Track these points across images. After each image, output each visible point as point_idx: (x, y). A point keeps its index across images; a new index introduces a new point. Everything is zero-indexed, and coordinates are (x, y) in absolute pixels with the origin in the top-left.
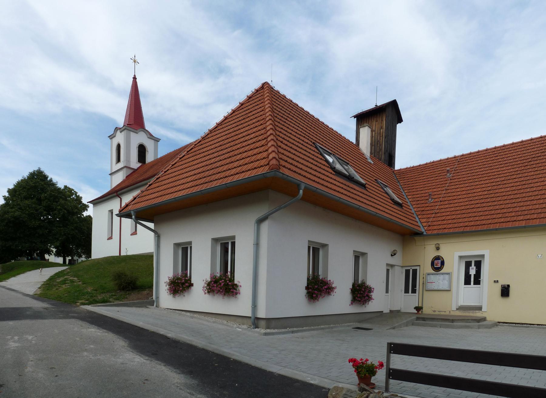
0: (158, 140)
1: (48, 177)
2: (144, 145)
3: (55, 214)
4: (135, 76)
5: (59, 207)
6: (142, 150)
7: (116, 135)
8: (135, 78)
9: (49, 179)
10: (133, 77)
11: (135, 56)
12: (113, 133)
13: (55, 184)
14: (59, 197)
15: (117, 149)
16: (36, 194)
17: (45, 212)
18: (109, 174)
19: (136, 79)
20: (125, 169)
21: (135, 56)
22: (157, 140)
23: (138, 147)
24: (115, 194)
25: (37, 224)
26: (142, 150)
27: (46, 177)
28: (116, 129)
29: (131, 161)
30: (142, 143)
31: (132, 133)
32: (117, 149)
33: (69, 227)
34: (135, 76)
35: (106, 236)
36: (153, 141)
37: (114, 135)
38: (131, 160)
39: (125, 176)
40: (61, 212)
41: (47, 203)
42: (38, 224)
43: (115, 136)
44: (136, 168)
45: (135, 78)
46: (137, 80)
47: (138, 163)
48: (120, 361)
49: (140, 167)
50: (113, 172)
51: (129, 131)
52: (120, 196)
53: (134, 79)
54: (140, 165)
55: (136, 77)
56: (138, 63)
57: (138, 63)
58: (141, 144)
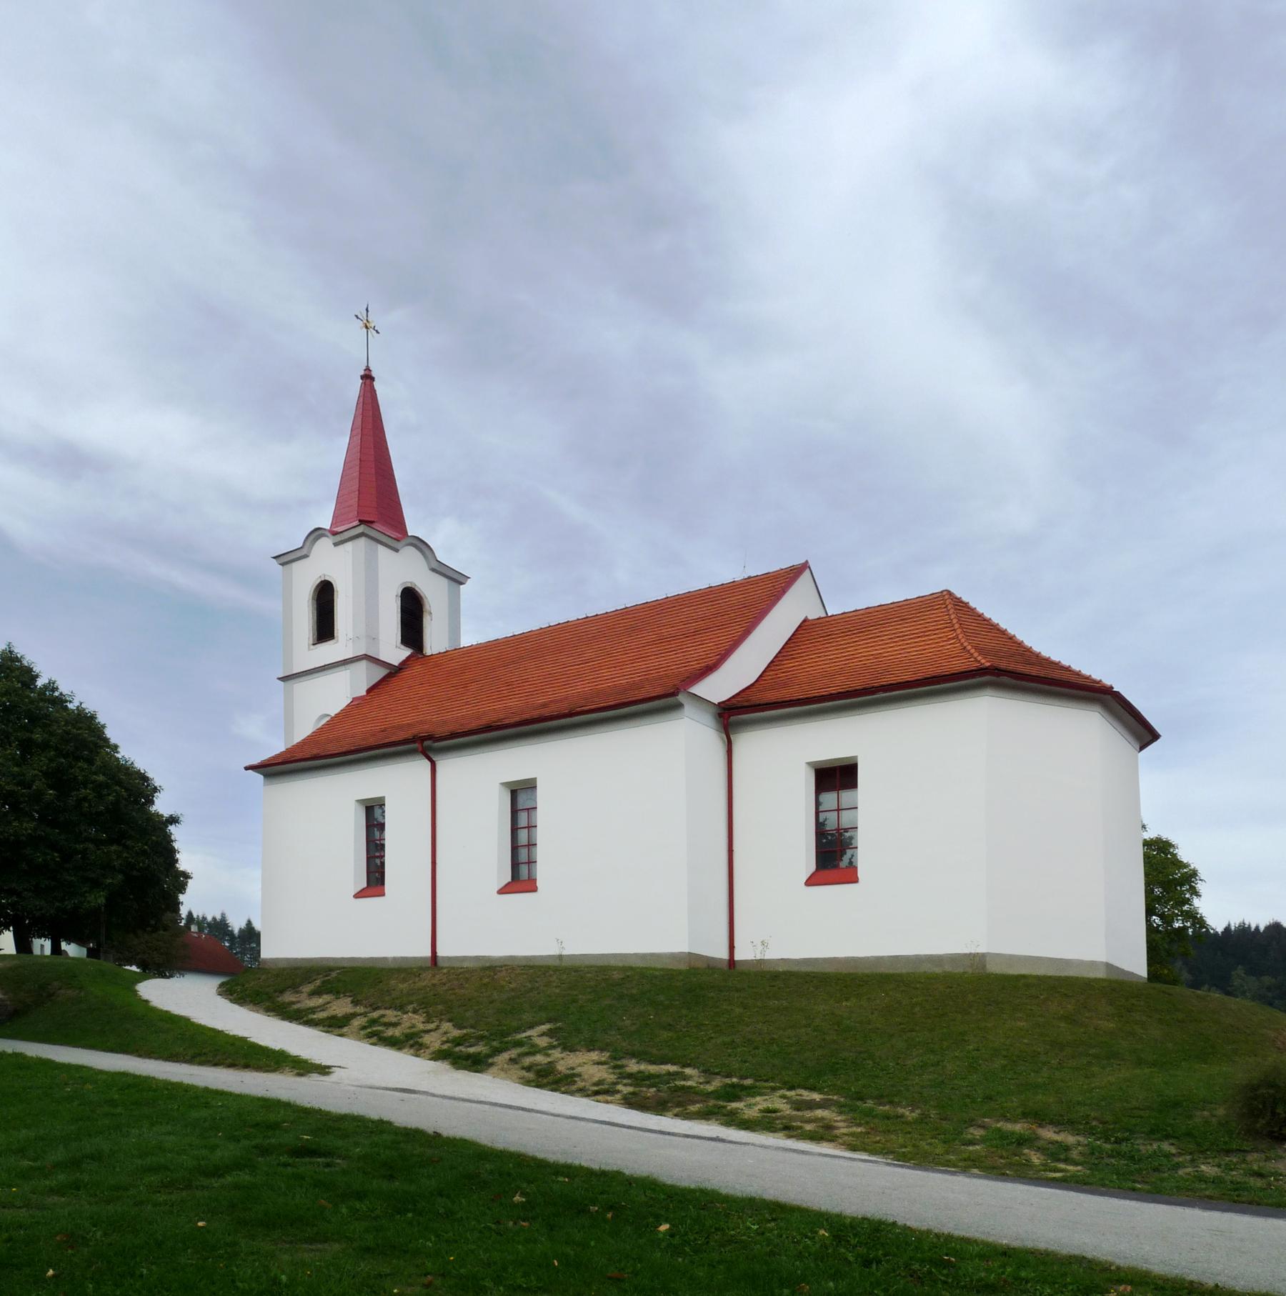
0: (461, 579)
1: (37, 676)
2: (417, 589)
3: (85, 799)
4: (368, 369)
5: (101, 778)
6: (412, 606)
7: (310, 552)
8: (368, 378)
9: (40, 683)
10: (362, 373)
11: (367, 310)
12: (300, 546)
13: (66, 701)
14: (91, 746)
15: (313, 599)
16: (11, 730)
17: (51, 792)
18: (279, 679)
19: (373, 379)
20: (363, 665)
21: (367, 310)
22: (456, 579)
23: (401, 596)
24: (415, 746)
25: (26, 830)
26: (412, 606)
27: (28, 676)
28: (317, 533)
29: (380, 638)
30: (411, 583)
31: (381, 548)
32: (316, 597)
33: (129, 843)
34: (368, 369)
35: (354, 872)
36: (444, 581)
37: (304, 552)
38: (382, 637)
39: (366, 689)
40: (109, 795)
41: (51, 760)
42: (30, 831)
43: (306, 556)
44: (396, 663)
45: (368, 378)
46: (374, 383)
47: (403, 647)
48: (1044, 1134)
49: (408, 659)
50: (294, 672)
51: (373, 543)
52: (432, 756)
53: (368, 381)
54: (406, 652)
55: (374, 374)
56: (378, 332)
57: (378, 332)
58: (409, 585)
